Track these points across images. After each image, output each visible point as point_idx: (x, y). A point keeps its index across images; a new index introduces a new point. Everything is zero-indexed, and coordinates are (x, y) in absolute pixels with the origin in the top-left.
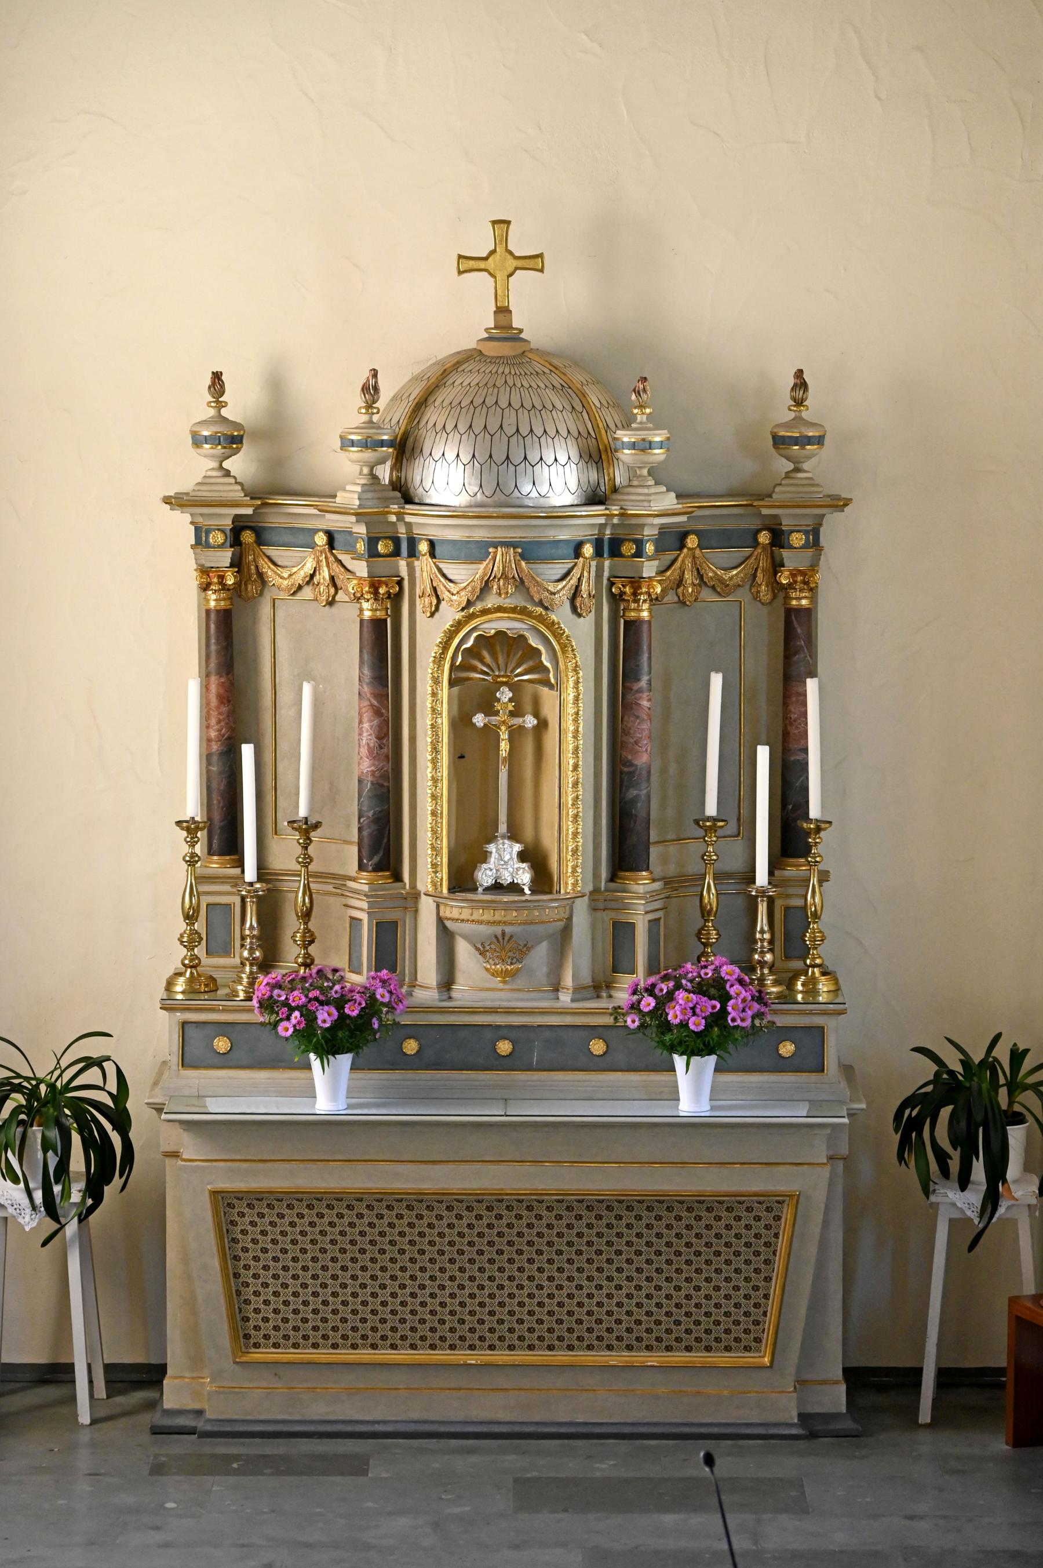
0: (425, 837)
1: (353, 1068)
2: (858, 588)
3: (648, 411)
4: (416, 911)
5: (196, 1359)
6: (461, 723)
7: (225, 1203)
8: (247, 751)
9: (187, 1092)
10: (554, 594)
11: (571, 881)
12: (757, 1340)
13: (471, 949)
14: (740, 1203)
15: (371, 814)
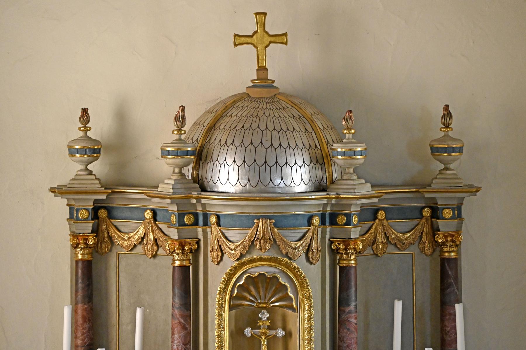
2: (484, 247)
3: (353, 131)
10: (295, 249)
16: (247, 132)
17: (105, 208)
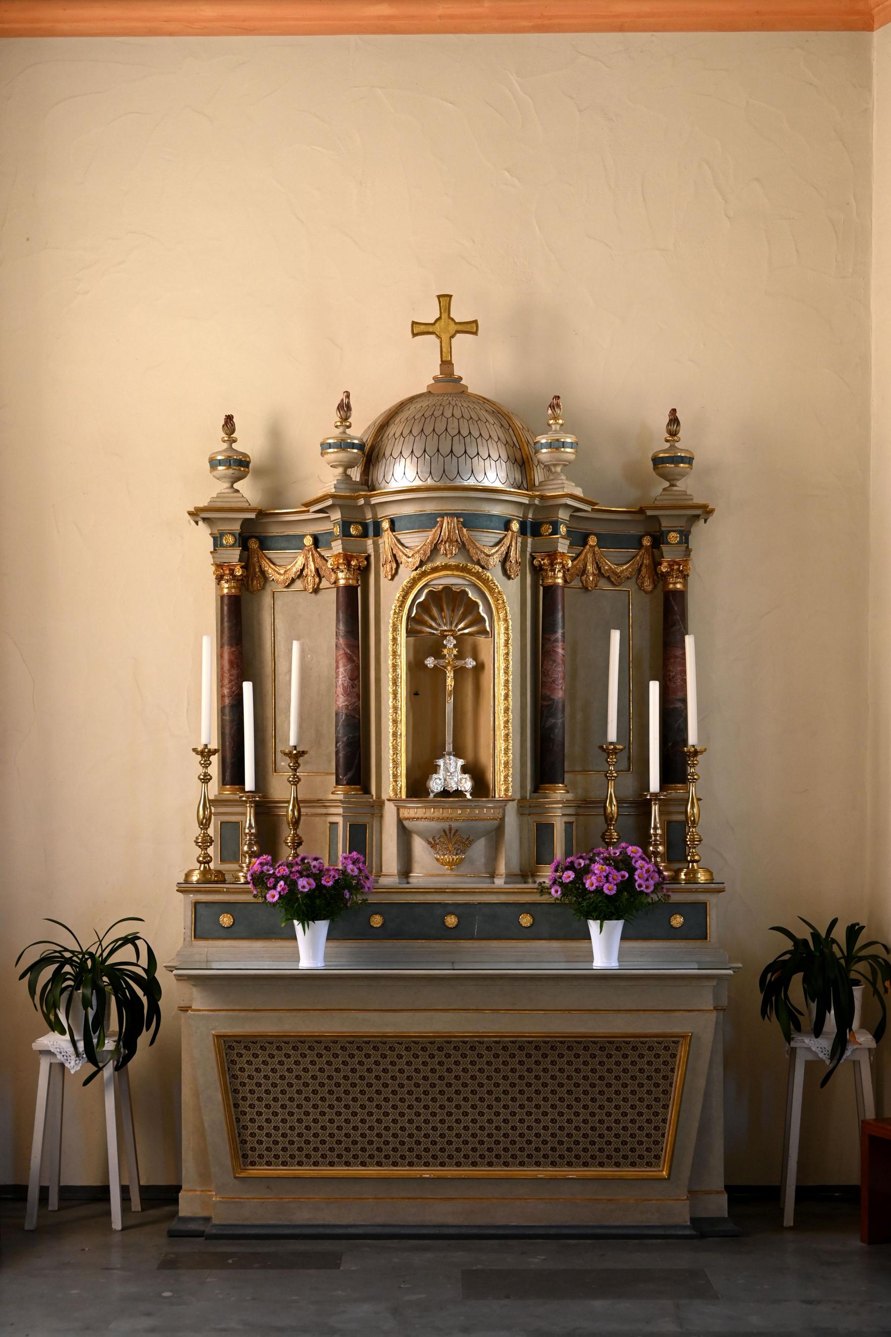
0: (388, 755)
1: (329, 938)
2: (720, 573)
3: (560, 422)
4: (381, 817)
5: (205, 1176)
6: (416, 667)
7: (230, 1048)
8: (247, 688)
9: (197, 958)
10: (489, 556)
11: (503, 788)
12: (657, 1157)
13: (424, 843)
14: (643, 1043)
15: (345, 739)
16: (428, 420)
17: (256, 537)
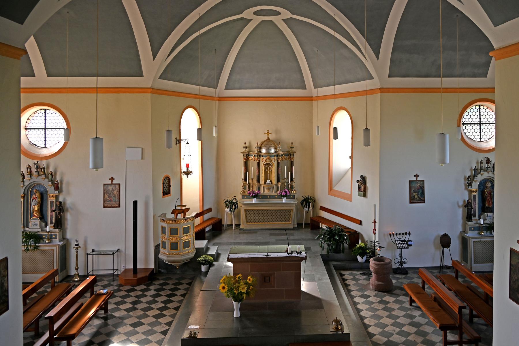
2: (296, 159)
5: (243, 224)
6: (265, 170)
